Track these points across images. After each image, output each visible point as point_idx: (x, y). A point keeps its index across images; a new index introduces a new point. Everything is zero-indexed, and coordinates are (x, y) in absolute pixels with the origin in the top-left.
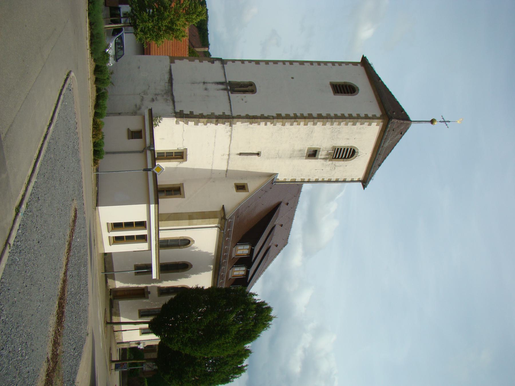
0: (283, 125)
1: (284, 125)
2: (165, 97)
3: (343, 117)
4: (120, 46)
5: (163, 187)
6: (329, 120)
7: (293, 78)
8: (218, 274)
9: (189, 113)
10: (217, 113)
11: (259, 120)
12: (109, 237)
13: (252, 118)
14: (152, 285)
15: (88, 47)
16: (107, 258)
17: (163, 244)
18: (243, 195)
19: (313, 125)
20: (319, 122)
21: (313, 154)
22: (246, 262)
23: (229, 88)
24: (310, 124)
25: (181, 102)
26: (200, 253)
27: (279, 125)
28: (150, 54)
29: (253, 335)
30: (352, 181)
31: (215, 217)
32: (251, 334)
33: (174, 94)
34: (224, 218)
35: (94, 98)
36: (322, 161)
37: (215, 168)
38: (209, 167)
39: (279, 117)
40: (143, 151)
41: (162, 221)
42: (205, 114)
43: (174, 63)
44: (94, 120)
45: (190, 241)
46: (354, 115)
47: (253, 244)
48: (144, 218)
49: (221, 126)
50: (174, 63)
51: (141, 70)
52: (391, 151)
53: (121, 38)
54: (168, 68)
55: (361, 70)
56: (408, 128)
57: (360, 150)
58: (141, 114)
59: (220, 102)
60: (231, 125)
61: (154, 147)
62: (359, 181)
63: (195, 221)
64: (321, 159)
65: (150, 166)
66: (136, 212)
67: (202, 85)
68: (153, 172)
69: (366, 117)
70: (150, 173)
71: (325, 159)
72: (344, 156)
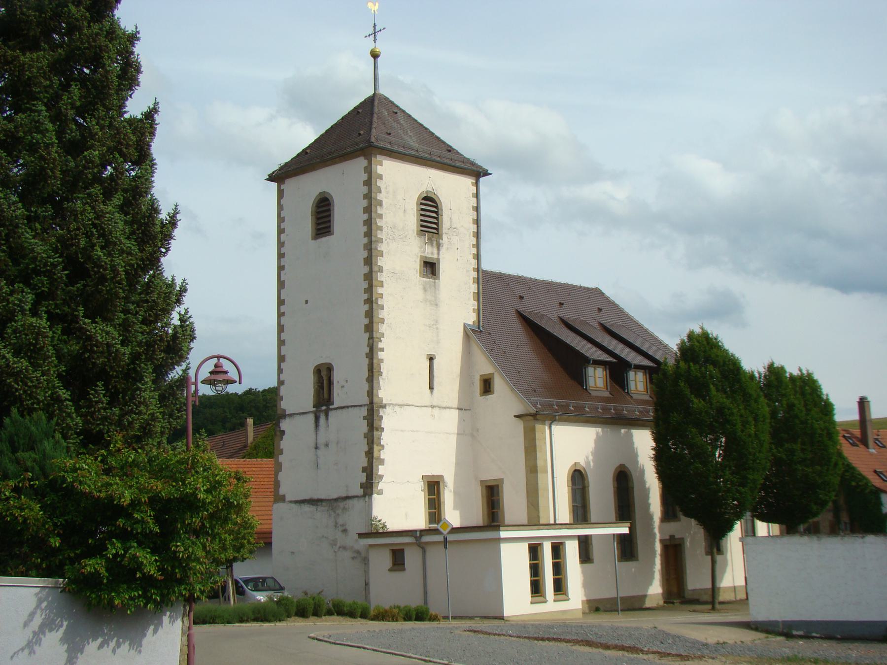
0: (382, 321)
1: (383, 319)
2: (339, 511)
3: (369, 223)
4: (260, 584)
5: (486, 513)
6: (373, 246)
7: (307, 302)
8: (638, 420)
9: (365, 474)
10: (365, 428)
11: (375, 361)
12: (555, 601)
13: (372, 372)
14: (656, 531)
15: (272, 624)
16: (595, 606)
17: (581, 512)
18: (499, 384)
19: (382, 272)
20: (376, 262)
21: (431, 267)
22: (618, 371)
23: (324, 408)
24: (381, 277)
25: (347, 486)
26: (597, 453)
27: (383, 328)
28: (271, 533)
29: (731, 367)
30: (477, 196)
31: (533, 430)
32: (730, 368)
33: (335, 496)
34: (535, 416)
35: (340, 618)
36: (443, 250)
37: (454, 429)
38: (453, 439)
39: (369, 328)
40: (423, 547)
41: (538, 517)
42: (366, 448)
43: (284, 496)
44: (372, 620)
45: (576, 471)
46: (365, 203)
47: (585, 361)
48: (524, 548)
49: (385, 423)
50: (284, 496)
51: (297, 549)
52: (426, 129)
53: (247, 581)
54: (293, 505)
55: (290, 185)
56: (386, 99)
57: (424, 189)
58: (368, 551)
59: (345, 424)
60: (384, 407)
61: (416, 531)
62: (477, 184)
63: (540, 463)
64: (438, 254)
65: (440, 538)
66: (514, 560)
67: (319, 452)
68: (449, 533)
69: (368, 183)
70: (451, 538)
71: (439, 246)
72: (434, 215)
